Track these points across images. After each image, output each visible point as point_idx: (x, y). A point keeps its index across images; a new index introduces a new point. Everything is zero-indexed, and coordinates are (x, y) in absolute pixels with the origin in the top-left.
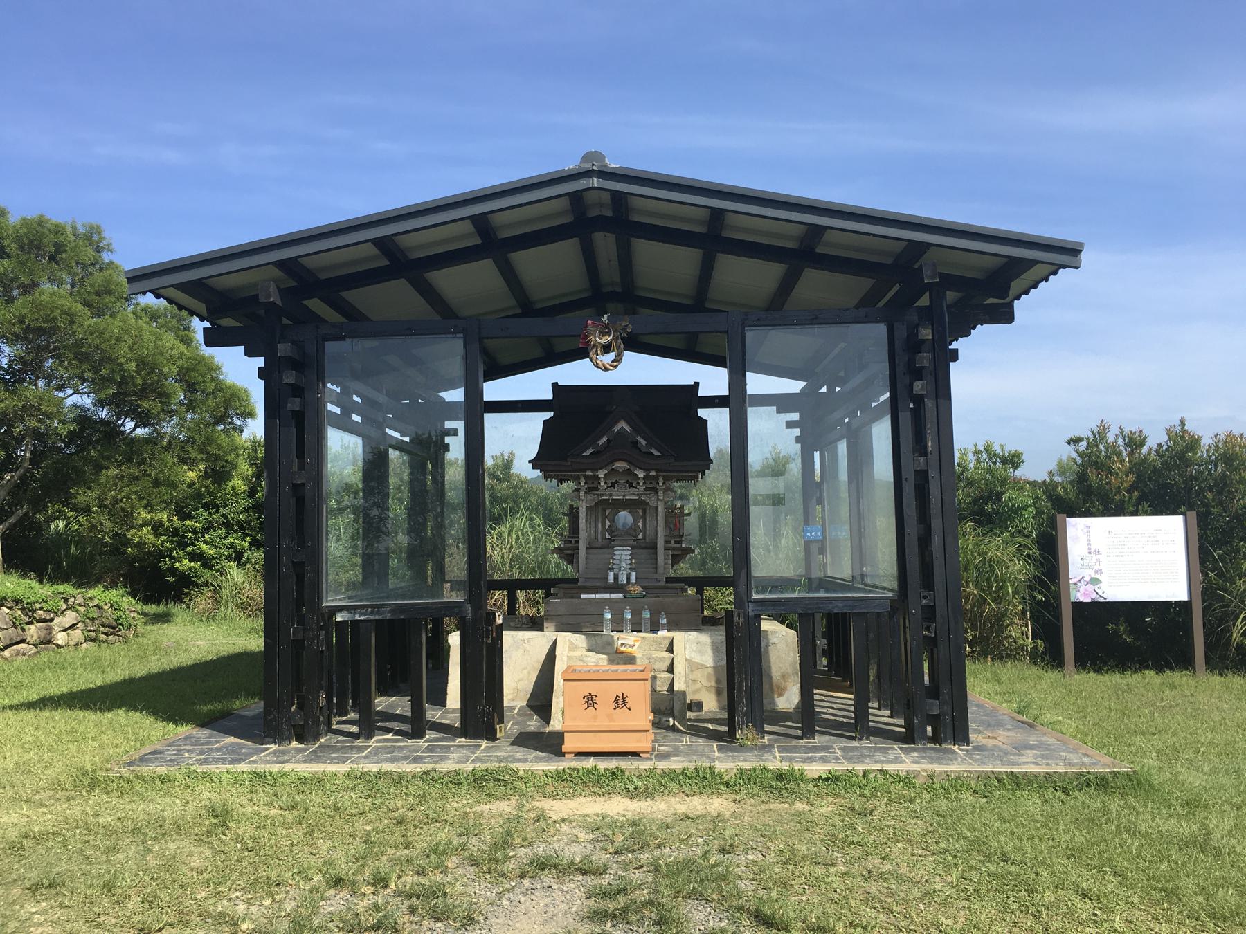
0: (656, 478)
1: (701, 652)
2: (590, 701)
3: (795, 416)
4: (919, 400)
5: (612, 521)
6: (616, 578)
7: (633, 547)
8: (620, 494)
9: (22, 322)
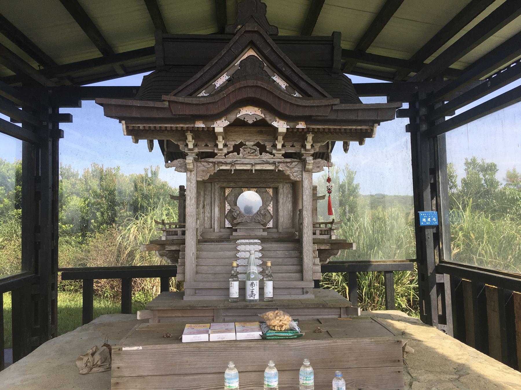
0: (301, 136)
6: (242, 289)
7: (264, 240)
8: (248, 161)
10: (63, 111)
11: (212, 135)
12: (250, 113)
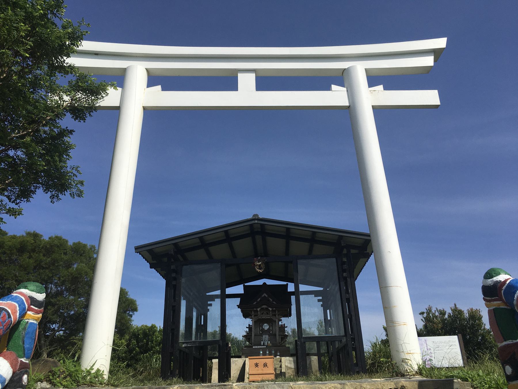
0: (275, 311)
1: (290, 363)
2: (257, 365)
3: (321, 298)
4: (345, 279)
5: (262, 327)
8: (264, 317)
9: (72, 275)
10: (209, 303)
11: (257, 311)
12: (264, 306)
